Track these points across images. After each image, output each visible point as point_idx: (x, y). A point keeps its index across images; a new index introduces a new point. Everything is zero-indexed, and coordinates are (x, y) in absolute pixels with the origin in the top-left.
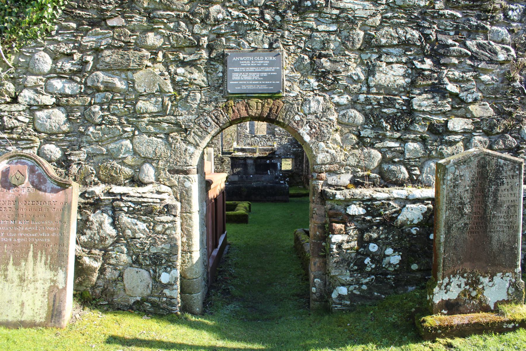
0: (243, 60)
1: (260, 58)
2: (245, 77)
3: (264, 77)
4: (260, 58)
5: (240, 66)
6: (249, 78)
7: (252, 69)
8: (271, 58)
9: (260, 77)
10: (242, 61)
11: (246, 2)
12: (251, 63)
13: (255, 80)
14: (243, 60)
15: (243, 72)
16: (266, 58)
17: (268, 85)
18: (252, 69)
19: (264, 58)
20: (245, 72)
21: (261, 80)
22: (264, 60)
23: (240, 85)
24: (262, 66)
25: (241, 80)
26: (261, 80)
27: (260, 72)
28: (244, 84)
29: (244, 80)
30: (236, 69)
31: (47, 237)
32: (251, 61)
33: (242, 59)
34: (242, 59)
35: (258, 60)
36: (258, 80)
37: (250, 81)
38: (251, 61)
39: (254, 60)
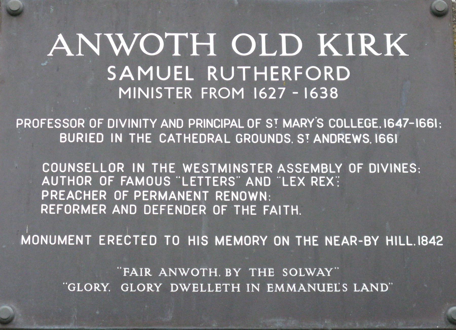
0: (137, 59)
1: (273, 44)
2: (153, 192)
3: (308, 196)
4: (273, 44)
5: (100, 99)
6: (188, 203)
7: (208, 130)
8: (367, 46)
9: (277, 193)
10: (121, 61)
11: (236, 3)
12: (200, 80)
13: (233, 222)
14: (137, 59)
15: (129, 153)
16: (325, 45)
17: (349, 264)
18: (208, 130)
19: (312, 45)
20: (156, 153)
21: (285, 225)
22: (310, 56)
23: (104, 263)
24: (292, 104)
25: (110, 223)
26: (285, 225)
27: (277, 154)
28: (136, 256)
29: (140, 223)
30: (72, 130)
31: (145, 280)
32: (198, 66)
33: (121, 46)
34: (121, 46)
35: (256, 61)
36: (259, 224)
37: (189, 225)
38: (198, 66)
39: (225, 58)
